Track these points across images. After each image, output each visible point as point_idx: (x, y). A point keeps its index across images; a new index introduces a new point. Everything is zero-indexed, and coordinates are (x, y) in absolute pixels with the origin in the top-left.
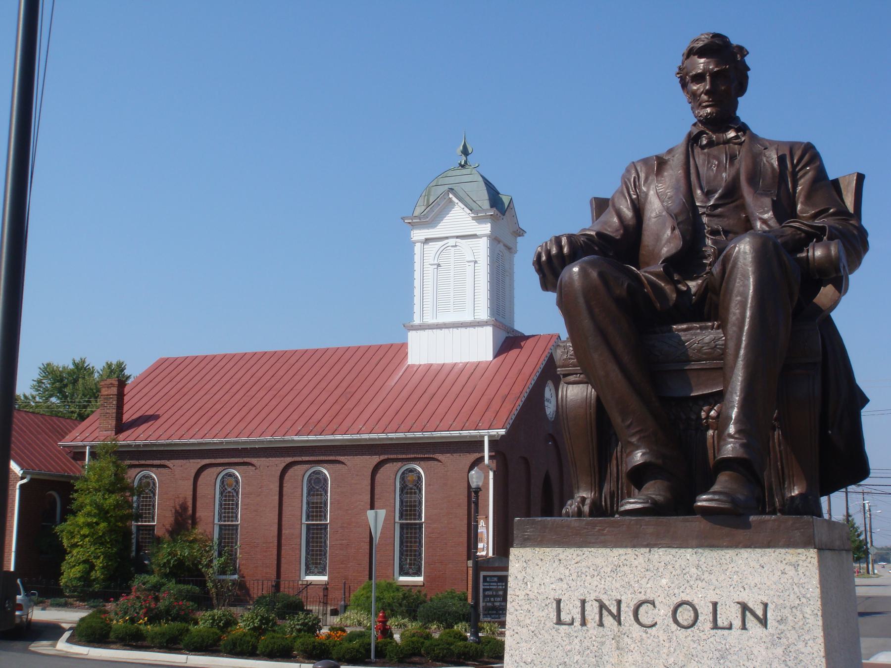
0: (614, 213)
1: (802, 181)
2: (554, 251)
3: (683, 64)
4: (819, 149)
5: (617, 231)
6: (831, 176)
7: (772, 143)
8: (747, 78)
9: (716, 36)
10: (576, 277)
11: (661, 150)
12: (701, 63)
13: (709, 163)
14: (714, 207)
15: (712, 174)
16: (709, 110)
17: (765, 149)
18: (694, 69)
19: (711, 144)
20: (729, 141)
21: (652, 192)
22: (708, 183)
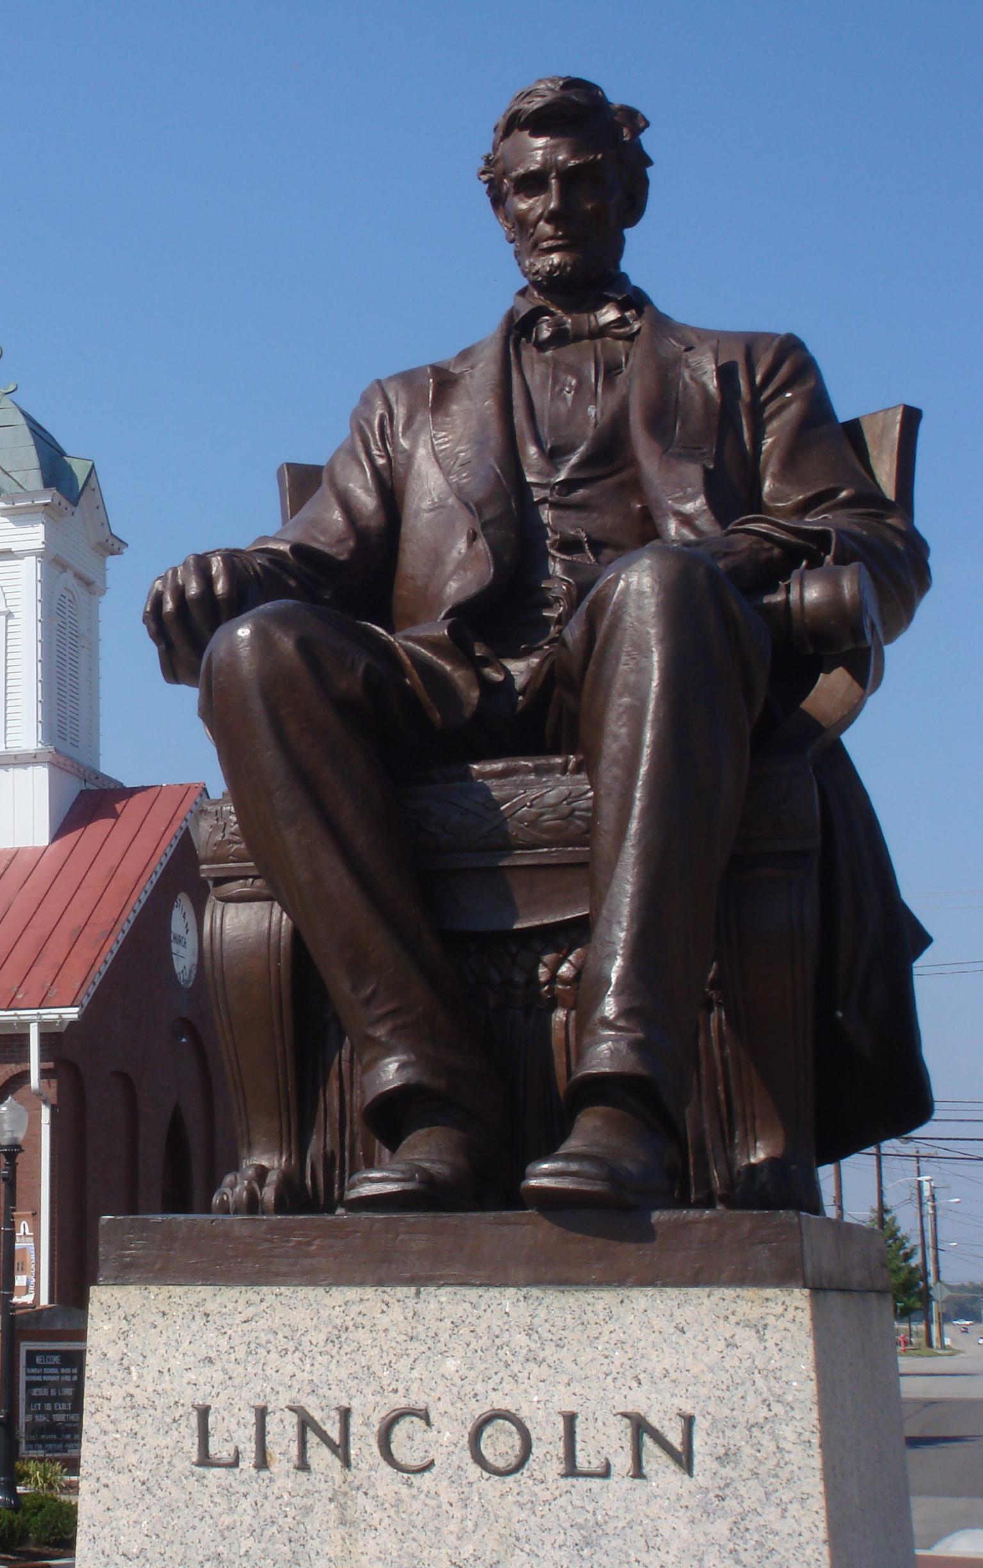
0: (333, 500)
1: (774, 424)
2: (193, 589)
3: (495, 149)
5: (341, 541)
6: (843, 415)
8: (645, 182)
10: (244, 651)
12: (538, 149)
13: (556, 381)
14: (569, 485)
15: (562, 408)
16: (555, 258)
17: (688, 349)
18: (521, 162)
19: (560, 338)
20: (602, 331)
21: (422, 452)
22: (554, 428)
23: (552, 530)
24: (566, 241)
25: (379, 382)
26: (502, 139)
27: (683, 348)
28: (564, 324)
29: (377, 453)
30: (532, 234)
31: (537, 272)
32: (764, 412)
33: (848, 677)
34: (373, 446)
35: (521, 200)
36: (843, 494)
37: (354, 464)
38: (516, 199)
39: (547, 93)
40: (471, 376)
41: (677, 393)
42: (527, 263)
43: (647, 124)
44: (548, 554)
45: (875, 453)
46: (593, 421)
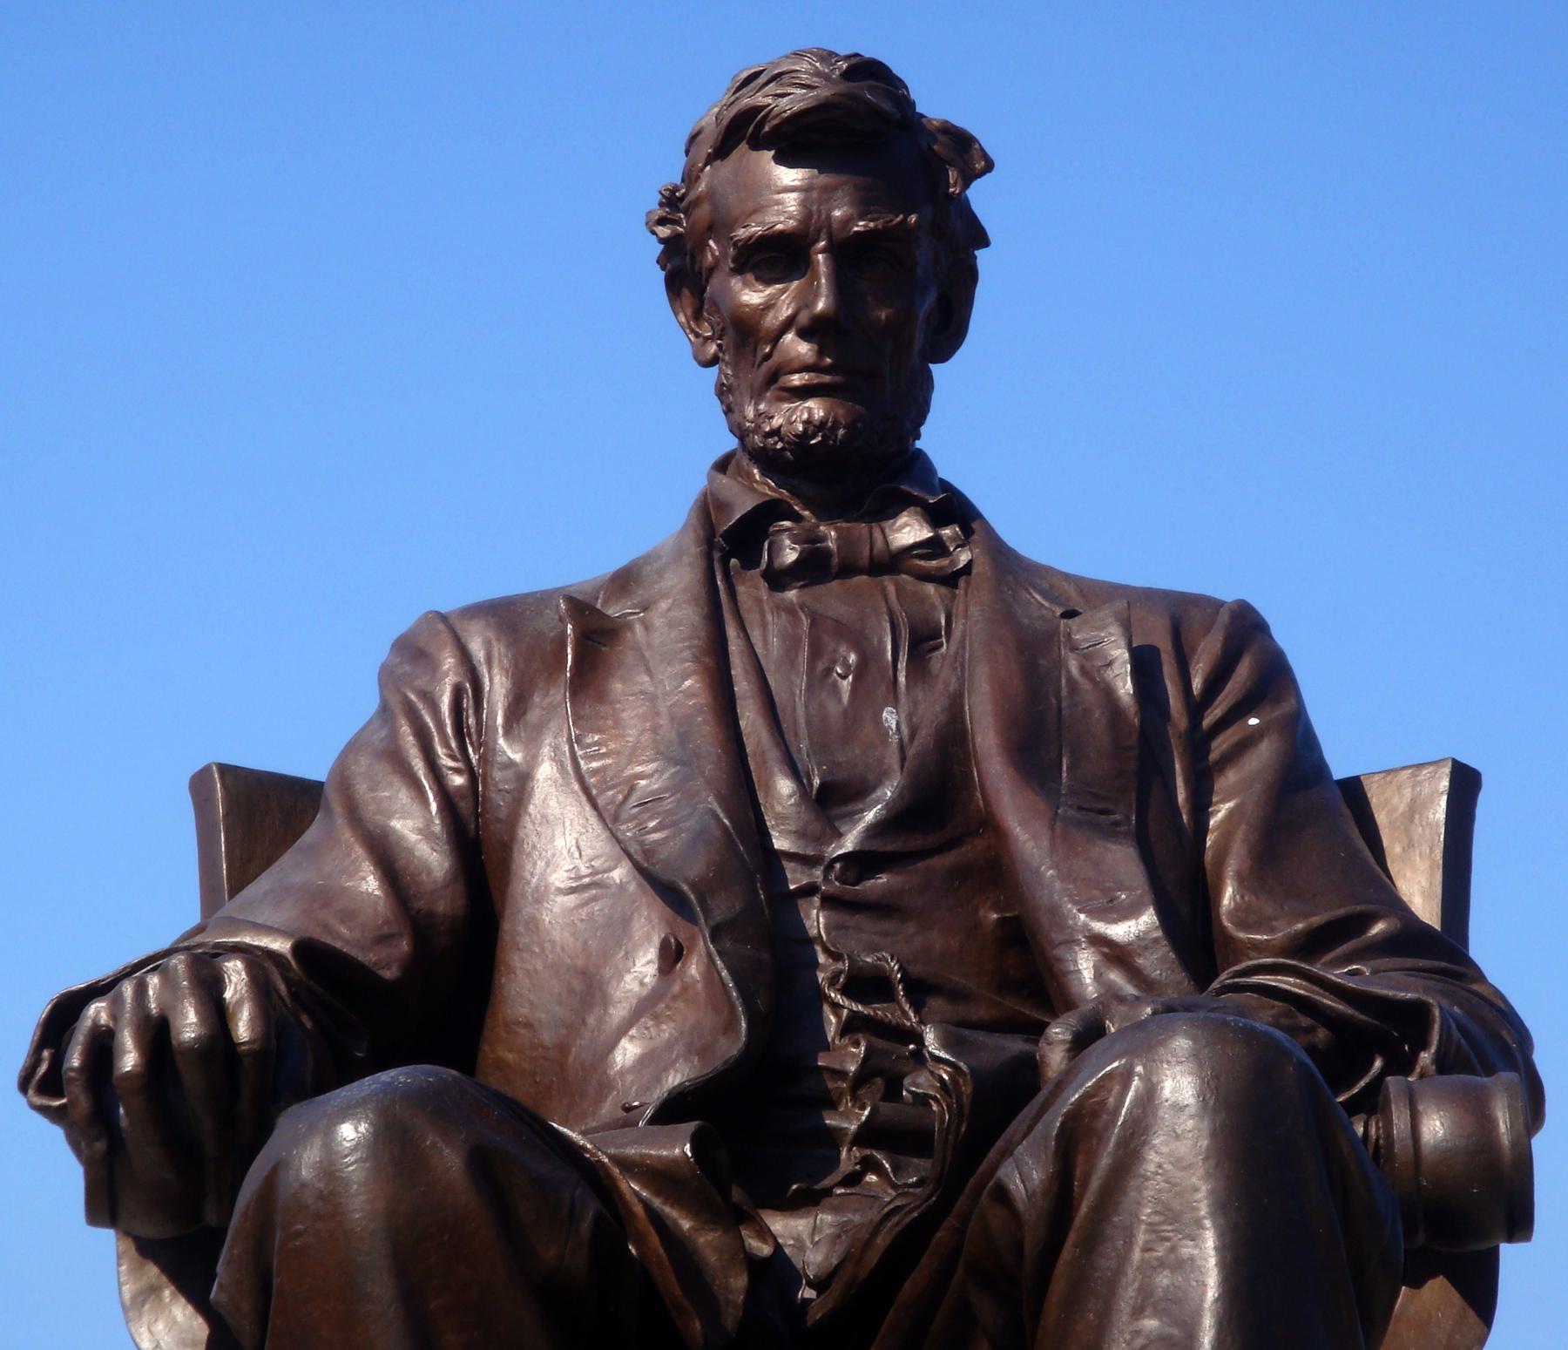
0: (359, 851)
1: (1230, 778)
2: (189, 1024)
3: (690, 177)
4: (1284, 634)
5: (382, 939)
6: (1339, 772)
7: (1097, 593)
8: (972, 275)
9: (867, 71)
10: (353, 1167)
11: (578, 564)
12: (786, 190)
13: (816, 652)
14: (861, 863)
15: (833, 709)
16: (816, 408)
17: (1070, 614)
18: (758, 210)
19: (814, 567)
20: (895, 561)
21: (545, 771)
22: (821, 747)
23: (826, 950)
24: (838, 379)
25: (443, 618)
26: (710, 160)
27: (1059, 611)
28: (824, 539)
29: (451, 764)
30: (768, 357)
31: (776, 432)
32: (1208, 751)
33: (1455, 1297)
34: (440, 750)
35: (746, 284)
36: (1378, 928)
37: (396, 780)
38: (735, 283)
39: (816, 81)
40: (647, 628)
41: (1059, 700)
42: (750, 412)
43: (989, 166)
44: (822, 997)
45: (1398, 849)
46: (895, 739)
